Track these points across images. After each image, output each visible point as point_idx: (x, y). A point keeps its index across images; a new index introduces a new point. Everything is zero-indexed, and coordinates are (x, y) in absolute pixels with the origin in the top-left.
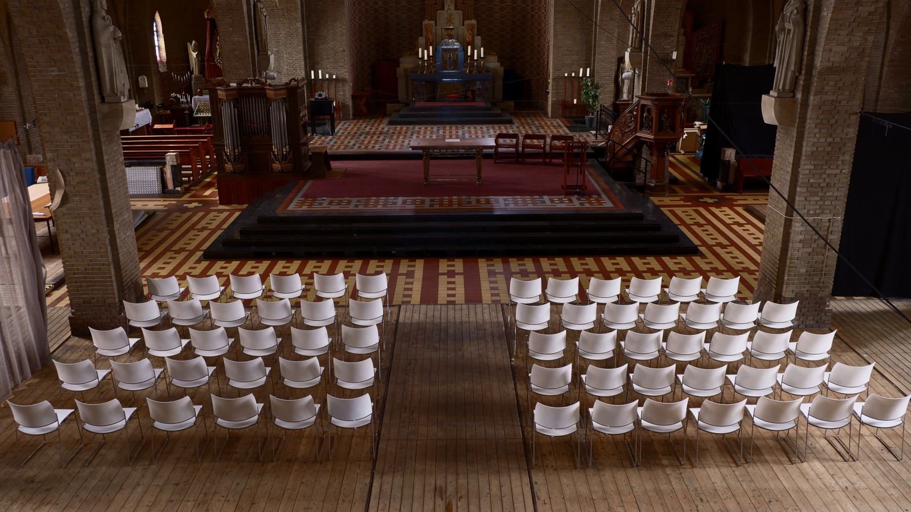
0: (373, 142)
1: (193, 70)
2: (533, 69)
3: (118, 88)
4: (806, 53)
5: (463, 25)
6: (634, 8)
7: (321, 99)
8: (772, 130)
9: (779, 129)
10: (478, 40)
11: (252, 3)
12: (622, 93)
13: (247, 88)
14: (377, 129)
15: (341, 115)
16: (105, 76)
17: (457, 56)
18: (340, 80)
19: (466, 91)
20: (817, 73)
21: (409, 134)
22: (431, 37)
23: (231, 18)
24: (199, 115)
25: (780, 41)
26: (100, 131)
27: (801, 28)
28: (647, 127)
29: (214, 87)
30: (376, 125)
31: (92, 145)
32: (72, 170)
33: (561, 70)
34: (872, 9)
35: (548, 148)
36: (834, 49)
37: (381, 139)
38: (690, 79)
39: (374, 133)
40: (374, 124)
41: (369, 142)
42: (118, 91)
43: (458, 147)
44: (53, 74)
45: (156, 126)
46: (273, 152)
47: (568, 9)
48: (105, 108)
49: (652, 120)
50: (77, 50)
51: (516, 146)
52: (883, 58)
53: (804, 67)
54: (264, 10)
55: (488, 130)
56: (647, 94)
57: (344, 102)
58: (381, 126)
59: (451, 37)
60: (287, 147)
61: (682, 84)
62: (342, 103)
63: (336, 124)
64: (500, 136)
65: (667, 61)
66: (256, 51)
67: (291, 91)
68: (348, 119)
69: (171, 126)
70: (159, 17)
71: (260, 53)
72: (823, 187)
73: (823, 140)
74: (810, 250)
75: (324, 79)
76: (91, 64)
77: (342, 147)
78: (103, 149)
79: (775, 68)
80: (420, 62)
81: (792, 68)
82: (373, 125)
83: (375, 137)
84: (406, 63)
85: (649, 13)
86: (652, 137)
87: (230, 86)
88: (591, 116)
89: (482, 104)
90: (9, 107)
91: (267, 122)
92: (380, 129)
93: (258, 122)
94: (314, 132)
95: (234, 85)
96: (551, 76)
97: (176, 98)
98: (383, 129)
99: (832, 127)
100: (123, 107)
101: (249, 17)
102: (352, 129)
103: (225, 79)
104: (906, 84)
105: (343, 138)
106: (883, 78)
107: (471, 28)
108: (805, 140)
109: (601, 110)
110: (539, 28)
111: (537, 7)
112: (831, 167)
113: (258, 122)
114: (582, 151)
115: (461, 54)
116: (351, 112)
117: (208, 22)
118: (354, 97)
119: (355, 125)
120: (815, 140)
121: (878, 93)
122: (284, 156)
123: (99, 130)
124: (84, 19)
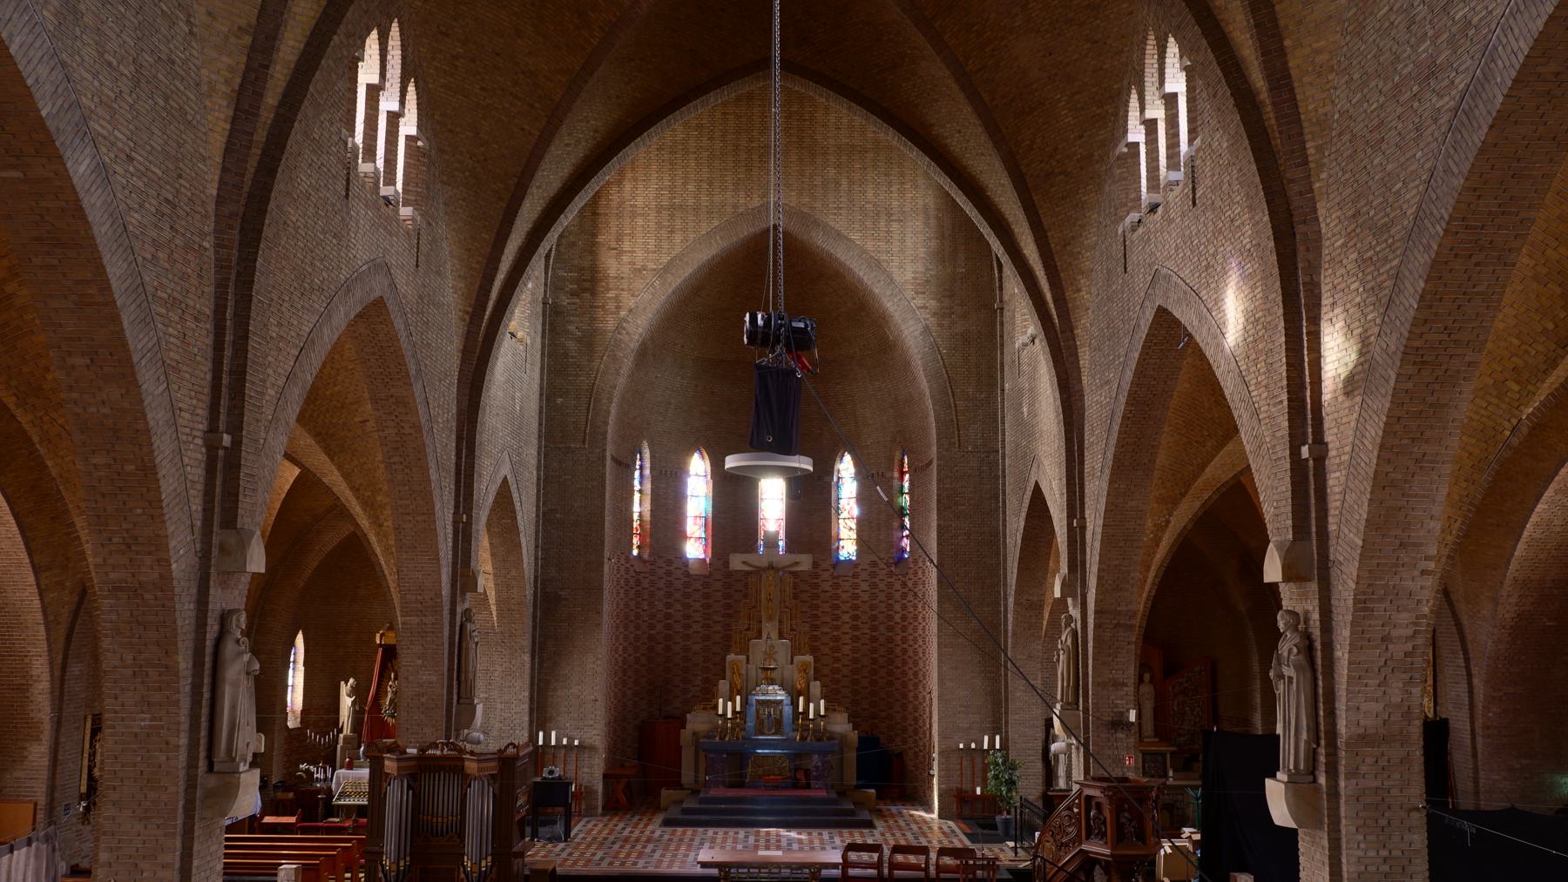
0: (634, 855)
4: (1321, 713)
5: (792, 663)
7: (553, 779)
8: (1290, 835)
9: (1300, 831)
10: (816, 687)
11: (458, 624)
12: (1057, 777)
13: (434, 757)
14: (642, 832)
15: (583, 807)
16: (221, 730)
17: (781, 712)
18: (585, 748)
19: (796, 770)
20: (1344, 744)
21: (696, 843)
22: (738, 682)
24: (342, 802)
26: (196, 817)
27: (1309, 675)
28: (1098, 834)
30: (641, 826)
31: (178, 843)
34: (1409, 647)
35: (932, 870)
36: (1364, 707)
37: (648, 850)
38: (1168, 756)
39: (637, 840)
40: (637, 824)
41: (628, 855)
42: (239, 753)
43: (779, 865)
44: (143, 723)
45: (268, 819)
46: (464, 867)
48: (212, 781)
49: (1104, 823)
50: (188, 689)
51: (878, 865)
52: (1472, 723)
53: (1322, 735)
54: (475, 633)
55: (832, 838)
56: (1094, 779)
58: (650, 828)
59: (771, 682)
60: (489, 859)
61: (1152, 763)
63: (572, 823)
64: (852, 847)
65: (1119, 723)
66: (455, 697)
67: (506, 765)
68: (596, 816)
69: (292, 820)
71: (461, 701)
73: (1372, 853)
75: (559, 746)
76: (205, 711)
77: (581, 863)
78: (195, 849)
79: (1279, 736)
81: (1304, 736)
82: (635, 826)
83: (639, 847)
84: (697, 722)
86: (1107, 851)
87: (406, 753)
88: (1005, 816)
89: (823, 794)
90: (31, 779)
92: (647, 833)
93: (445, 815)
94: (534, 835)
95: (412, 751)
96: (936, 749)
97: (307, 771)
98: (653, 832)
101: (451, 644)
102: (600, 832)
103: (400, 743)
104: (1518, 766)
105: (583, 846)
106: (1479, 754)
107: (804, 669)
108: (1344, 853)
109: (1022, 805)
111: (912, 637)
113: (445, 815)
114: (989, 875)
115: (787, 710)
116: (600, 803)
119: (605, 825)
120: (1361, 853)
121: (1476, 781)
122: (483, 874)
123: (194, 816)
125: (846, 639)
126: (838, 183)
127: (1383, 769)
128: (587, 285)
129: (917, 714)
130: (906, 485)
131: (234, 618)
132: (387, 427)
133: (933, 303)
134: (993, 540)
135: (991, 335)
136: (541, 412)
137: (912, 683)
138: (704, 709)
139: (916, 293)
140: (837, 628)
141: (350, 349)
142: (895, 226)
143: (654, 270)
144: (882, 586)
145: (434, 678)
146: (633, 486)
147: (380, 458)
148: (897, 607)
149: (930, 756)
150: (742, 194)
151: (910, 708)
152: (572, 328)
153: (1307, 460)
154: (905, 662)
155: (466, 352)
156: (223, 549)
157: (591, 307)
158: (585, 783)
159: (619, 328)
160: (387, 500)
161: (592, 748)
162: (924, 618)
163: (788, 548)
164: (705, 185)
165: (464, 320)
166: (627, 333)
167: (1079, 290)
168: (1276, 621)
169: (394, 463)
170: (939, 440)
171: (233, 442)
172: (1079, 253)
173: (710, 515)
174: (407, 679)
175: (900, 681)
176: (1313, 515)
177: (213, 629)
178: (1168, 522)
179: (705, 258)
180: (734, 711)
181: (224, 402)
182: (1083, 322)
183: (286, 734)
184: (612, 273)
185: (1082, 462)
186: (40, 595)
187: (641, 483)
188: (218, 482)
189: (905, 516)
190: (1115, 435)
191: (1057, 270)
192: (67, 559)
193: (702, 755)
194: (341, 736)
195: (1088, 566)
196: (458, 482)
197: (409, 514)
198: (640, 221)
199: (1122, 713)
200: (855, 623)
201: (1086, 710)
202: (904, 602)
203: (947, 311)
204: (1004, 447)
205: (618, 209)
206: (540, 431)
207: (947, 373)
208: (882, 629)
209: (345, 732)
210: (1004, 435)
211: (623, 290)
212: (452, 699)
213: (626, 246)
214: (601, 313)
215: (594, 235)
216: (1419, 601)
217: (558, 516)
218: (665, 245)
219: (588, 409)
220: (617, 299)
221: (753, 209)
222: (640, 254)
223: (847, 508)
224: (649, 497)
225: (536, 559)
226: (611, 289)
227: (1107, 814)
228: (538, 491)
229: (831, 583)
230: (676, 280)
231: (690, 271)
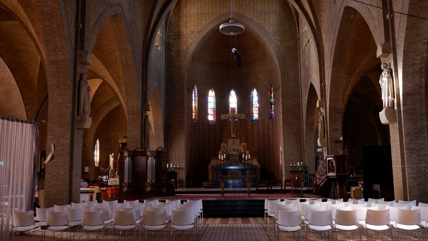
1: (110, 167)
2: (275, 168)
3: (86, 110)
5: (240, 145)
6: (319, 119)
8: (386, 127)
11: (144, 119)
23: (134, 124)
25: (382, 88)
28: (332, 170)
29: (123, 151)
32: (58, 144)
33: (288, 163)
34: (420, 66)
38: (354, 169)
44: (60, 100)
47: (290, 135)
48: (79, 118)
57: (182, 179)
60: (155, 180)
62: (181, 180)
65: (338, 141)
66: (143, 139)
70: (99, 142)
71: (145, 141)
72: (417, 150)
73: (412, 127)
74: (418, 183)
76: (76, 98)
80: (219, 162)
85: (327, 121)
91: (146, 168)
99: (414, 121)
100: (87, 118)
110: (277, 148)
111: (275, 139)
112: (419, 140)
117: (121, 144)
118: (187, 178)
120: (408, 127)
124: (77, 80)
125: (256, 142)
126: (250, 5)
127: (414, 103)
128: (177, 37)
129: (277, 161)
130: (272, 96)
131: (84, 75)
132: (123, 58)
133: (279, 38)
134: (299, 106)
135: (296, 46)
136: (165, 73)
137: (276, 152)
138: (215, 159)
139: (274, 35)
140: (253, 139)
141: (112, 34)
142: (267, 16)
143: (197, 32)
144: (266, 126)
145: (137, 133)
146: (192, 98)
147: (121, 69)
148: (271, 131)
149: (282, 170)
150: (222, 9)
151: (276, 160)
152: (173, 49)
153: (388, 19)
154: (273, 147)
155: (144, 42)
156: (80, 55)
157: (179, 43)
158: (181, 179)
159: (187, 48)
160: (123, 81)
161: (182, 169)
162: (279, 133)
163: (238, 112)
164: (211, 7)
165: (143, 32)
166: (190, 50)
167: (321, 16)
168: (381, 67)
169: (125, 69)
170: (281, 77)
171: (82, 27)
172: (321, 5)
173: (215, 108)
174: (130, 134)
175: (272, 153)
176: (391, 34)
177: (78, 78)
178: (350, 81)
179: (212, 28)
180: (224, 159)
181: (80, 16)
182: (323, 25)
183: (95, 168)
184: (185, 33)
185: (324, 67)
186: (26, 112)
187: (195, 98)
188: (79, 37)
189: (272, 105)
190: (333, 53)
191: (315, 11)
192: (33, 102)
193: (214, 171)
194: (110, 170)
195: (327, 96)
196: (143, 79)
197: (129, 85)
198: (192, 18)
199: (338, 138)
200: (258, 137)
201: (327, 138)
202: (273, 129)
203: (283, 40)
204: (301, 78)
205: (186, 15)
206: (165, 78)
207: (283, 58)
208: (266, 138)
209: (111, 168)
210: (301, 75)
211: (188, 38)
212: (143, 140)
213: (189, 25)
214: (181, 44)
215: (179, 23)
216: (423, 52)
217: (171, 102)
218: (200, 24)
219: (179, 72)
220: (186, 40)
221: (225, 13)
222: (193, 27)
223: (255, 104)
224: (197, 102)
225: (165, 115)
226: (184, 38)
227: (334, 164)
228: (165, 95)
229: (251, 126)
230: (203, 34)
231: (207, 31)
